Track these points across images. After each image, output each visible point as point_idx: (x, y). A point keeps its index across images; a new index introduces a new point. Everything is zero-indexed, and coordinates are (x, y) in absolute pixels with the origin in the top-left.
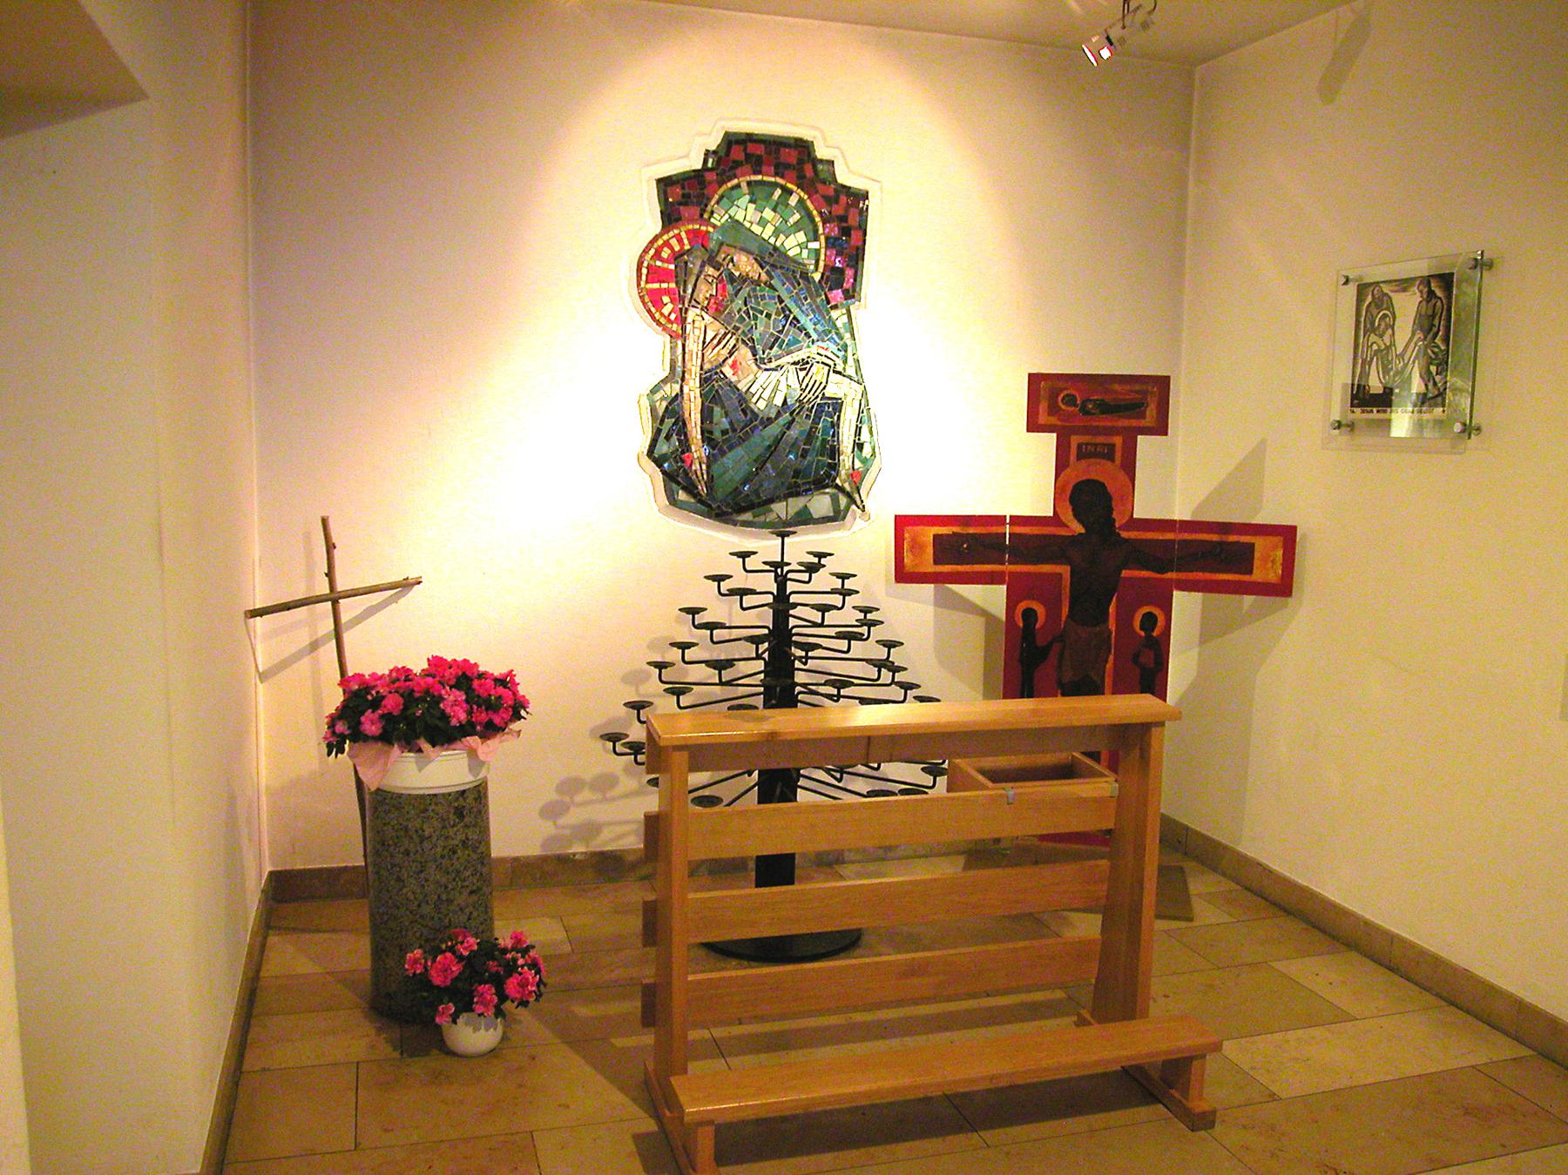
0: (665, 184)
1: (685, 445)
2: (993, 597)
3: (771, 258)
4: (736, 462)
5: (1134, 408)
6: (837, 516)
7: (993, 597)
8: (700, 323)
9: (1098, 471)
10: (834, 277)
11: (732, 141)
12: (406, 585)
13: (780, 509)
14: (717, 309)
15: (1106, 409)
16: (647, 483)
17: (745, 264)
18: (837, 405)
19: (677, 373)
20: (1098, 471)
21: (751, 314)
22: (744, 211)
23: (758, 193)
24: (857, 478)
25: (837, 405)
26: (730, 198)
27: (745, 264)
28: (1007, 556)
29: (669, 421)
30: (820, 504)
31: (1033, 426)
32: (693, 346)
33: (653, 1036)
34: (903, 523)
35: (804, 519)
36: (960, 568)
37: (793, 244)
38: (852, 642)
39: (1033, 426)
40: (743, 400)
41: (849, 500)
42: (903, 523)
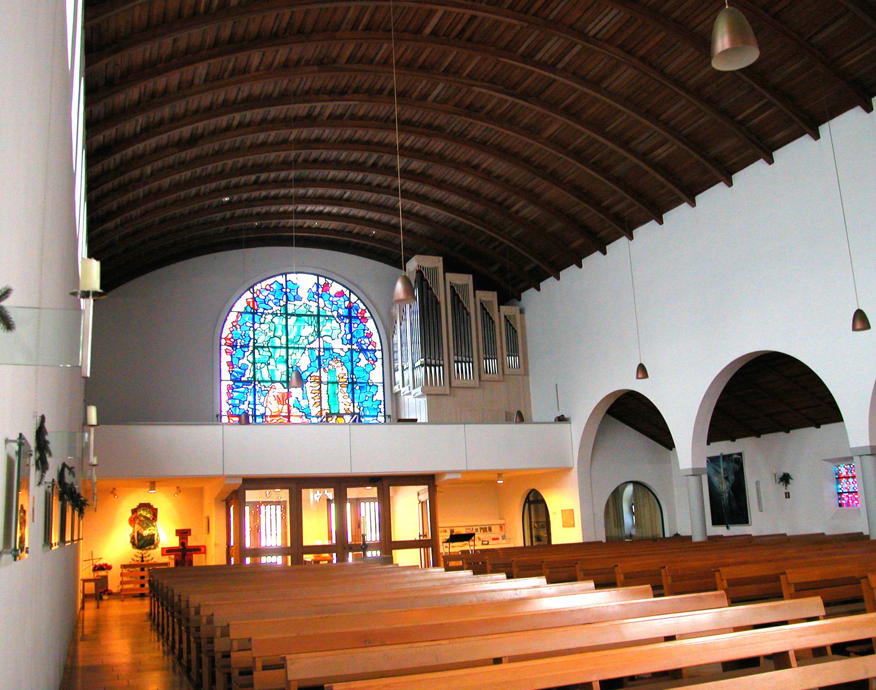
0: (132, 510)
1: (135, 541)
2: (173, 556)
3: (145, 517)
4: (142, 542)
5: (187, 533)
6: (155, 548)
7: (173, 556)
8: (136, 526)
9: (183, 540)
10: (153, 519)
11: (140, 504)
12: (101, 558)
13: (147, 548)
14: (139, 524)
15: (184, 533)
16: (130, 545)
17: (142, 518)
18: (154, 535)
19: (134, 532)
20: (183, 540)
21: (143, 524)
22: (142, 512)
23: (143, 510)
24: (157, 544)
25: (154, 535)
26: (140, 511)
27: (142, 518)
28: (227, 199)
29: (133, 538)
30: (152, 547)
31: (176, 535)
32: (136, 528)
33: (80, 664)
34: (162, 549)
35: (150, 549)
36: (81, 346)
37: (148, 516)
38: (522, 545)
39: (176, 535)
40: (142, 535)
41: (156, 546)
42: (162, 549)
